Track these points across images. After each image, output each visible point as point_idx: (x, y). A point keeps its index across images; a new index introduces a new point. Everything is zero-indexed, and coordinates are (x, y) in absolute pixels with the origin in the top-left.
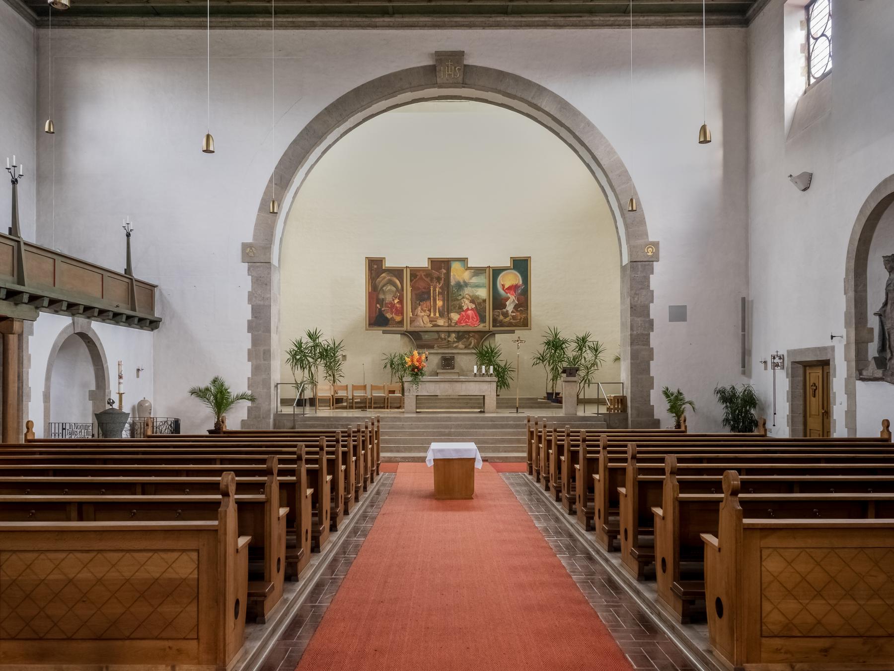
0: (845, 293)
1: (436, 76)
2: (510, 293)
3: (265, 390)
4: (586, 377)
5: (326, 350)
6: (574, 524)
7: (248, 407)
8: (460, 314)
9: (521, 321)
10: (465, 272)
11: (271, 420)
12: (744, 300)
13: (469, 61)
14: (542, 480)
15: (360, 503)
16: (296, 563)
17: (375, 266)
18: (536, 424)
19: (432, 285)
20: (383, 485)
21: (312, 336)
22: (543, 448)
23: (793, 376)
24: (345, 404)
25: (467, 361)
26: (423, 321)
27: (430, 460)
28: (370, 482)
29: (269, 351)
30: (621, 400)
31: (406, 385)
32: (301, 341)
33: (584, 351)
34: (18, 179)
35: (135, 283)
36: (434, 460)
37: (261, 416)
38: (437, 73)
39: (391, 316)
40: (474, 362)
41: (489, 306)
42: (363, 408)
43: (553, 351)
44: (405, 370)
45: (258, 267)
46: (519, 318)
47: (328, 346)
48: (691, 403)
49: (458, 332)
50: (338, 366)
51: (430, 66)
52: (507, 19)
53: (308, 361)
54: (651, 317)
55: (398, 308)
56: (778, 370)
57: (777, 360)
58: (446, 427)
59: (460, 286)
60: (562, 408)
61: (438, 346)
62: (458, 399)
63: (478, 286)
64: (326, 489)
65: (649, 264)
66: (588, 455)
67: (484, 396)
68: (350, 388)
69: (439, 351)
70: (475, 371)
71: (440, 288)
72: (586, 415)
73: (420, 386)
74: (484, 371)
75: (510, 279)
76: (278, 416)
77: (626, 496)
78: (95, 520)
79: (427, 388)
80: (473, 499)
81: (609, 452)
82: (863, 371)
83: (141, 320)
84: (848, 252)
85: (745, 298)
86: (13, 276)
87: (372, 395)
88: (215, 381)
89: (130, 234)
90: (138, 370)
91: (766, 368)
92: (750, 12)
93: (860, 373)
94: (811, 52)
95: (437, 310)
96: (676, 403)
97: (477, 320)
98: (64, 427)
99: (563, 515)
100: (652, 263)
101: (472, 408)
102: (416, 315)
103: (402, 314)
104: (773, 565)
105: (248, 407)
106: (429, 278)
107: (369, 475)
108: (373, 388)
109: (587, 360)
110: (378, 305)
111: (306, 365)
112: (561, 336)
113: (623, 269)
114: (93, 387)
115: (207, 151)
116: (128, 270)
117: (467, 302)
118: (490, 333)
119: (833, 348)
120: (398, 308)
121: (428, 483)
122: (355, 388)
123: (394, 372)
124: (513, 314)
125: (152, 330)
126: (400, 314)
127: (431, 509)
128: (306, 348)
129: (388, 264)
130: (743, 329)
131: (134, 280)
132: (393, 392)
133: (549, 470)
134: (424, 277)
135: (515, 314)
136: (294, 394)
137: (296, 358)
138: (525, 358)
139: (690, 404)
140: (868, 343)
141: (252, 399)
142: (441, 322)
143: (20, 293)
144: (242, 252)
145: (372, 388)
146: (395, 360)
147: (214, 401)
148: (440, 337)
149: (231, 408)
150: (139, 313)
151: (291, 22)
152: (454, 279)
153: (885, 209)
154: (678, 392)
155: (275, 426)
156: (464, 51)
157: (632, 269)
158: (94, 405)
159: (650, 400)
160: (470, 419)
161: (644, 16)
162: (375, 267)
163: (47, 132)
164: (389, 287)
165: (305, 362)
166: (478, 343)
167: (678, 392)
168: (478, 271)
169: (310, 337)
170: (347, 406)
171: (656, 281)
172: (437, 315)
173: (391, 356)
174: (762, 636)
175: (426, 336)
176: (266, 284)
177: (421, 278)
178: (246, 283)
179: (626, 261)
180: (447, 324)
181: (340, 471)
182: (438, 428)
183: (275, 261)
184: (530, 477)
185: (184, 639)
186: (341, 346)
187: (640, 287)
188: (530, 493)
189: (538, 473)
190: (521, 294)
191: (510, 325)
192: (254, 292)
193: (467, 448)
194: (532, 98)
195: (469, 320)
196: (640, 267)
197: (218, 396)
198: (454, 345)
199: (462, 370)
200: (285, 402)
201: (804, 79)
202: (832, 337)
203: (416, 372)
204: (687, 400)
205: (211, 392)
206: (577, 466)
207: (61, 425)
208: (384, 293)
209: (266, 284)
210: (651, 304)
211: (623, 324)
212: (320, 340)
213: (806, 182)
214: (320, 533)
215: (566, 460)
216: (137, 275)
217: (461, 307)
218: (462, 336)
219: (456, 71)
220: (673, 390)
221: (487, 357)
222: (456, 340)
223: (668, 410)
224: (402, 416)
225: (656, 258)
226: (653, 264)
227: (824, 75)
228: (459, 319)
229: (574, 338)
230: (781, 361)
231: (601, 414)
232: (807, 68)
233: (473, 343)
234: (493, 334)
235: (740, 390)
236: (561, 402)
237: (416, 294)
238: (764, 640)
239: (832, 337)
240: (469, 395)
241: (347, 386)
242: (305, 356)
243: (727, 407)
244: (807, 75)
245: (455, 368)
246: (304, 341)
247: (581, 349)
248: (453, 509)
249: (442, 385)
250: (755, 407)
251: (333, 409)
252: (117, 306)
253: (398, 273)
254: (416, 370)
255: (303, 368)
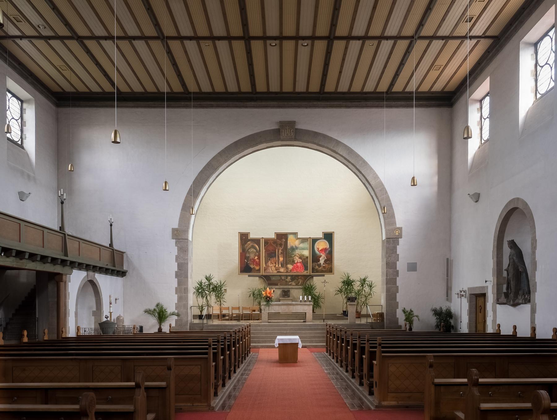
0: (493, 259)
1: (280, 135)
2: (322, 253)
3: (185, 310)
4: (365, 302)
5: (216, 287)
6: (355, 382)
7: (176, 319)
8: (293, 265)
9: (329, 269)
10: (295, 241)
11: (188, 327)
12: (448, 259)
13: (299, 126)
14: (357, 377)
15: (244, 364)
16: (217, 388)
17: (244, 238)
18: (333, 328)
19: (277, 248)
20: (253, 358)
21: (208, 279)
22: (350, 350)
23: (470, 302)
24: (227, 318)
25: (297, 293)
26: (271, 269)
27: (277, 344)
28: (233, 373)
29: (187, 288)
30: (381, 315)
31: (262, 307)
32: (201, 281)
33: (364, 286)
34: (64, 201)
35: (115, 251)
36: (279, 344)
37: (183, 325)
38: (280, 133)
39: (253, 267)
40: (301, 294)
41: (310, 261)
42: (238, 320)
43: (347, 287)
44: (261, 298)
45: (181, 242)
46: (327, 267)
47: (217, 284)
48: (417, 316)
49: (292, 276)
50: (223, 295)
51: (277, 129)
52: (319, 103)
53: (205, 293)
54: (398, 269)
55: (257, 262)
56: (463, 298)
57: (463, 293)
58: (285, 330)
59: (293, 249)
60: (348, 319)
61: (280, 284)
62: (292, 315)
63: (303, 249)
64: (221, 363)
65: (396, 240)
66: (383, 354)
67: (306, 313)
68: (230, 309)
69: (281, 287)
70: (301, 299)
71: (281, 250)
72: (362, 323)
73: (270, 308)
74: (306, 299)
75: (322, 245)
76: (192, 325)
77: (376, 365)
78: (93, 382)
79: (275, 308)
80: (297, 363)
81: (383, 347)
82: (499, 299)
83: (118, 272)
84: (494, 237)
85: (448, 258)
86: (62, 252)
87: (243, 312)
88: (157, 305)
89: (112, 225)
90: (116, 299)
91: (458, 298)
92: (453, 100)
93: (498, 301)
94: (538, 76)
95: (280, 263)
96: (409, 316)
97: (303, 269)
98: (85, 330)
99: (338, 368)
100: (398, 239)
101: (299, 320)
102: (268, 266)
103: (260, 265)
104: (392, 369)
105: (176, 319)
106: (275, 244)
107: (237, 364)
108: (243, 308)
109: (366, 292)
110: (246, 260)
111: (204, 295)
112: (351, 278)
113: (383, 241)
114: (95, 309)
115: (165, 190)
116: (111, 245)
117: (297, 258)
118: (310, 277)
119: (487, 287)
120: (257, 262)
121: (275, 355)
122: (233, 308)
123: (255, 299)
124: (324, 265)
125: (122, 277)
126: (258, 266)
127: (277, 367)
128: (204, 286)
129: (252, 236)
130: (447, 276)
131: (66, 235)
132: (254, 311)
133: (354, 364)
134: (272, 244)
135: (324, 265)
136: (198, 312)
137: (199, 291)
138: (331, 290)
139: (417, 317)
140: (503, 285)
141: (178, 315)
142: (282, 270)
143: (66, 261)
144: (172, 233)
145: (243, 309)
146: (256, 292)
147: (158, 316)
148: (281, 278)
149: (167, 320)
150: (117, 268)
151: (199, 104)
152: (290, 245)
153: (511, 216)
154: (411, 310)
155: (190, 329)
156: (295, 121)
157: (387, 243)
158: (95, 319)
159: (396, 315)
160: (298, 325)
161: (395, 102)
162: (244, 238)
163: (69, 171)
164: (252, 250)
165: (204, 294)
166: (303, 282)
167: (411, 310)
168: (304, 240)
169: (206, 279)
170: (229, 319)
171: (400, 249)
172: (280, 266)
173: (253, 290)
174: (388, 393)
175: (274, 278)
176: (186, 251)
177: (271, 245)
178: (175, 251)
179: (384, 238)
180: (285, 271)
181: (211, 366)
182: (280, 330)
183: (190, 239)
184: (326, 354)
185: (196, 395)
186: (225, 284)
187: (391, 252)
188: (327, 360)
189: (337, 358)
190: (328, 254)
191: (322, 271)
192: (179, 256)
193: (295, 338)
194: (333, 147)
195: (298, 269)
196: (391, 241)
197: (161, 313)
198: (290, 283)
199: (294, 298)
200: (195, 317)
201: (533, 95)
202: (486, 281)
203: (268, 300)
204: (415, 314)
205: (156, 311)
206: (356, 351)
207: (83, 329)
208: (249, 253)
209: (186, 251)
210: (397, 262)
211: (383, 273)
212: (213, 281)
213: (477, 198)
214: (218, 386)
215: (350, 348)
216: (116, 247)
217: (293, 261)
218: (294, 278)
219: (291, 132)
220: (408, 309)
221: (308, 290)
222: (290, 280)
223: (404, 320)
224: (260, 324)
225: (400, 236)
226: (398, 240)
227: (547, 92)
228: (292, 268)
229: (359, 279)
230: (465, 293)
231: (368, 322)
232: (480, 134)
233: (300, 282)
234: (312, 277)
235: (444, 309)
236: (347, 316)
237: (267, 254)
238: (389, 394)
239: (486, 281)
240: (297, 313)
241: (229, 307)
242: (204, 290)
243: (437, 318)
244: (480, 138)
245: (290, 297)
246: (203, 281)
247: (362, 286)
248: (287, 366)
249: (283, 307)
250: (452, 318)
251: (221, 321)
252: (107, 265)
253: (257, 241)
254: (268, 299)
255: (203, 297)
